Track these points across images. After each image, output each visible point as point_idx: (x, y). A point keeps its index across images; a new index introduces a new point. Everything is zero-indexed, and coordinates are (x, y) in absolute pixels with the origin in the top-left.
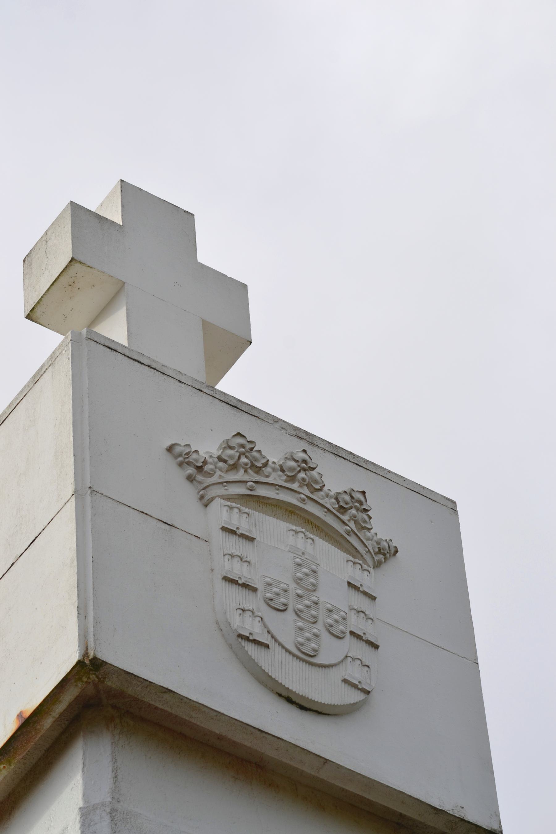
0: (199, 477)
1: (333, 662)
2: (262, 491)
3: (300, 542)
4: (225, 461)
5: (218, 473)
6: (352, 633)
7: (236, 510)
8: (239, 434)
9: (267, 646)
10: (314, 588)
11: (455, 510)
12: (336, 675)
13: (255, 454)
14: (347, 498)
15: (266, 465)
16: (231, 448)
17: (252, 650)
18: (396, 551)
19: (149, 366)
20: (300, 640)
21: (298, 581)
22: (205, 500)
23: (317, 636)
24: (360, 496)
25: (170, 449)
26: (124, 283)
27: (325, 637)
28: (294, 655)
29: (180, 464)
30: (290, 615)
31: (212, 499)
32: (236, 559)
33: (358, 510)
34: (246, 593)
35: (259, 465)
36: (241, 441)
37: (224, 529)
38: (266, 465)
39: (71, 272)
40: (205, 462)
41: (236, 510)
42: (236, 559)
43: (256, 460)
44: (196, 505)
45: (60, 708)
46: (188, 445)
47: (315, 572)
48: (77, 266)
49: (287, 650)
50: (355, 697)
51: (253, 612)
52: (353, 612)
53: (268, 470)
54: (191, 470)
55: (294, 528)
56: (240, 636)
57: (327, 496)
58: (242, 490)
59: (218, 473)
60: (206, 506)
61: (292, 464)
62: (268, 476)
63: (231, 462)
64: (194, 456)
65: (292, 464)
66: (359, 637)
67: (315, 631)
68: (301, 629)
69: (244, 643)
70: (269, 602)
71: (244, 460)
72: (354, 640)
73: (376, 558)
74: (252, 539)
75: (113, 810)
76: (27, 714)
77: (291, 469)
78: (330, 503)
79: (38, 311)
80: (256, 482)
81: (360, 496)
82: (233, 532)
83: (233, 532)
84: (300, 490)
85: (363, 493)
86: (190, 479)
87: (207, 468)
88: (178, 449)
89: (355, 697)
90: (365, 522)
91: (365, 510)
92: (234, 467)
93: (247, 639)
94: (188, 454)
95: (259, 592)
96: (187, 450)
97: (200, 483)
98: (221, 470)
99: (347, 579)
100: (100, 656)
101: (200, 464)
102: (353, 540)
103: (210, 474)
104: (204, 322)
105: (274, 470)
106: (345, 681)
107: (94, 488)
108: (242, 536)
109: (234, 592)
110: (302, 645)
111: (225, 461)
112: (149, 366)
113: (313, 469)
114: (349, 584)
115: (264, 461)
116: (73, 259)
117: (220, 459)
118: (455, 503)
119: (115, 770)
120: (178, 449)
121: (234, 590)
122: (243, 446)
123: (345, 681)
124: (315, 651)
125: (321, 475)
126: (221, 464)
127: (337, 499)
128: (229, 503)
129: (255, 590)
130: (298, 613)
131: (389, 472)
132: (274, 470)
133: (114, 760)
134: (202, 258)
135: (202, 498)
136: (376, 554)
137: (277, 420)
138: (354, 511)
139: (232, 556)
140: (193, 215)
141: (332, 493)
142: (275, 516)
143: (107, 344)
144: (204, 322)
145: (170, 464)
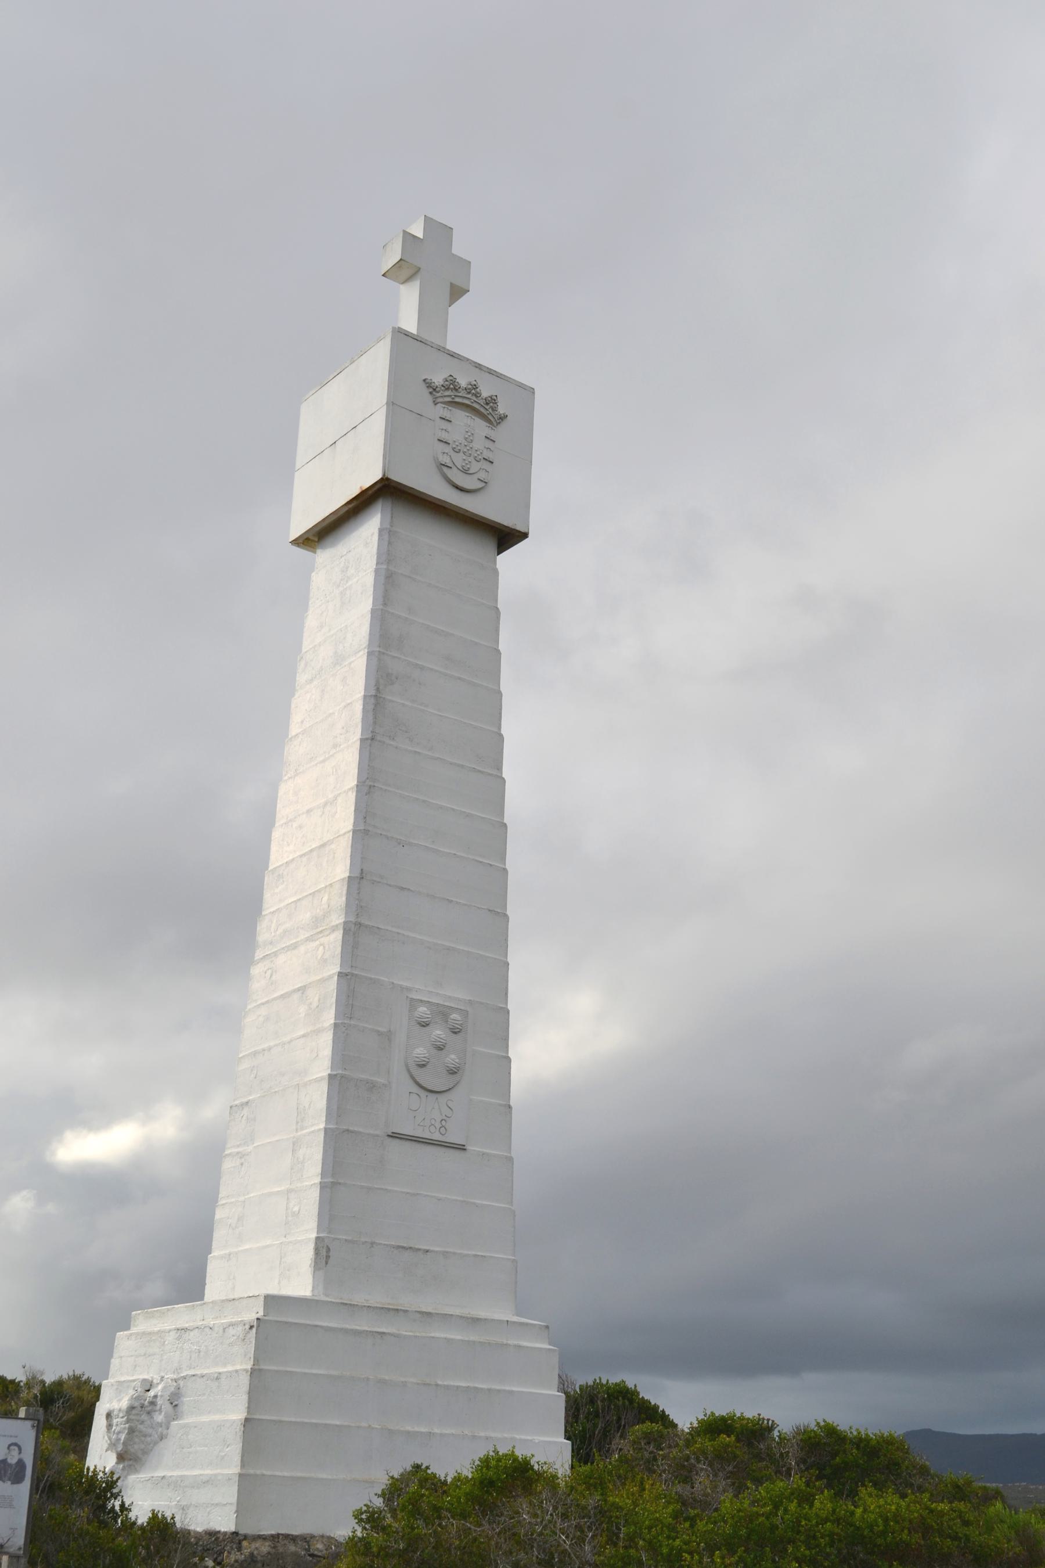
0: (434, 393)
1: (476, 471)
2: (457, 400)
3: (469, 421)
4: (444, 387)
5: (441, 392)
6: (484, 458)
7: (446, 409)
8: (451, 376)
9: (451, 468)
10: (472, 441)
11: (534, 393)
12: (476, 476)
13: (456, 384)
14: (490, 399)
15: (460, 388)
16: (447, 381)
17: (445, 469)
18: (507, 416)
19: (421, 341)
20: (464, 464)
21: (466, 439)
22: (436, 402)
23: (470, 462)
24: (495, 398)
25: (424, 380)
26: (420, 269)
27: (474, 462)
28: (461, 471)
29: (428, 387)
30: (461, 454)
31: (438, 403)
32: (443, 431)
33: (493, 403)
34: (446, 445)
35: (457, 388)
36: (451, 378)
37: (441, 418)
38: (460, 388)
39: (400, 263)
40: (437, 387)
41: (446, 409)
42: (443, 431)
43: (456, 386)
44: (432, 404)
45: (375, 488)
46: (431, 380)
47: (472, 434)
48: (402, 262)
49: (458, 468)
50: (481, 485)
51: (447, 453)
52: (485, 449)
53: (460, 390)
54: (431, 390)
55: (467, 414)
56: (441, 464)
57: (482, 399)
58: (449, 399)
59: (441, 392)
60: (436, 404)
61: (470, 387)
62: (460, 392)
63: (446, 387)
64: (433, 384)
65: (470, 387)
66: (486, 460)
67: (470, 460)
68: (464, 460)
69: (442, 467)
70: (453, 449)
71: (452, 386)
72: (484, 461)
73: (498, 421)
74: (450, 421)
75: (390, 531)
76: (364, 489)
77: (469, 389)
78: (482, 402)
79: (387, 274)
80: (455, 396)
81: (495, 398)
82: (444, 419)
83: (444, 419)
84: (471, 398)
85: (496, 396)
86: (431, 393)
87: (438, 389)
88: (427, 381)
89: (481, 485)
90: (495, 408)
91: (496, 403)
92: (448, 389)
93: (444, 465)
94: (431, 383)
95: (451, 445)
96: (430, 381)
97: (434, 395)
98: (442, 390)
99: (485, 435)
100: (389, 477)
101: (435, 388)
102: (490, 417)
103: (438, 392)
104: (451, 284)
105: (463, 390)
106: (479, 479)
107: (394, 402)
108: (447, 420)
109: (442, 445)
110: (464, 466)
111: (444, 387)
112: (421, 341)
113: (477, 388)
114: (486, 437)
115: (459, 386)
116: (401, 259)
117: (442, 386)
118: (534, 389)
119: (392, 514)
120: (427, 381)
121: (442, 444)
122: (452, 380)
123: (479, 479)
124: (469, 468)
125: (480, 390)
126: (443, 388)
127: (486, 400)
128: (444, 406)
129: (449, 444)
130: (464, 453)
131: (510, 378)
132: (463, 390)
133: (392, 510)
134: (456, 250)
135: (434, 401)
136: (498, 419)
137: (468, 360)
138: (491, 404)
139: (442, 429)
140: (452, 229)
141: (484, 398)
142: (461, 410)
143: (406, 333)
144: (451, 284)
145: (424, 386)
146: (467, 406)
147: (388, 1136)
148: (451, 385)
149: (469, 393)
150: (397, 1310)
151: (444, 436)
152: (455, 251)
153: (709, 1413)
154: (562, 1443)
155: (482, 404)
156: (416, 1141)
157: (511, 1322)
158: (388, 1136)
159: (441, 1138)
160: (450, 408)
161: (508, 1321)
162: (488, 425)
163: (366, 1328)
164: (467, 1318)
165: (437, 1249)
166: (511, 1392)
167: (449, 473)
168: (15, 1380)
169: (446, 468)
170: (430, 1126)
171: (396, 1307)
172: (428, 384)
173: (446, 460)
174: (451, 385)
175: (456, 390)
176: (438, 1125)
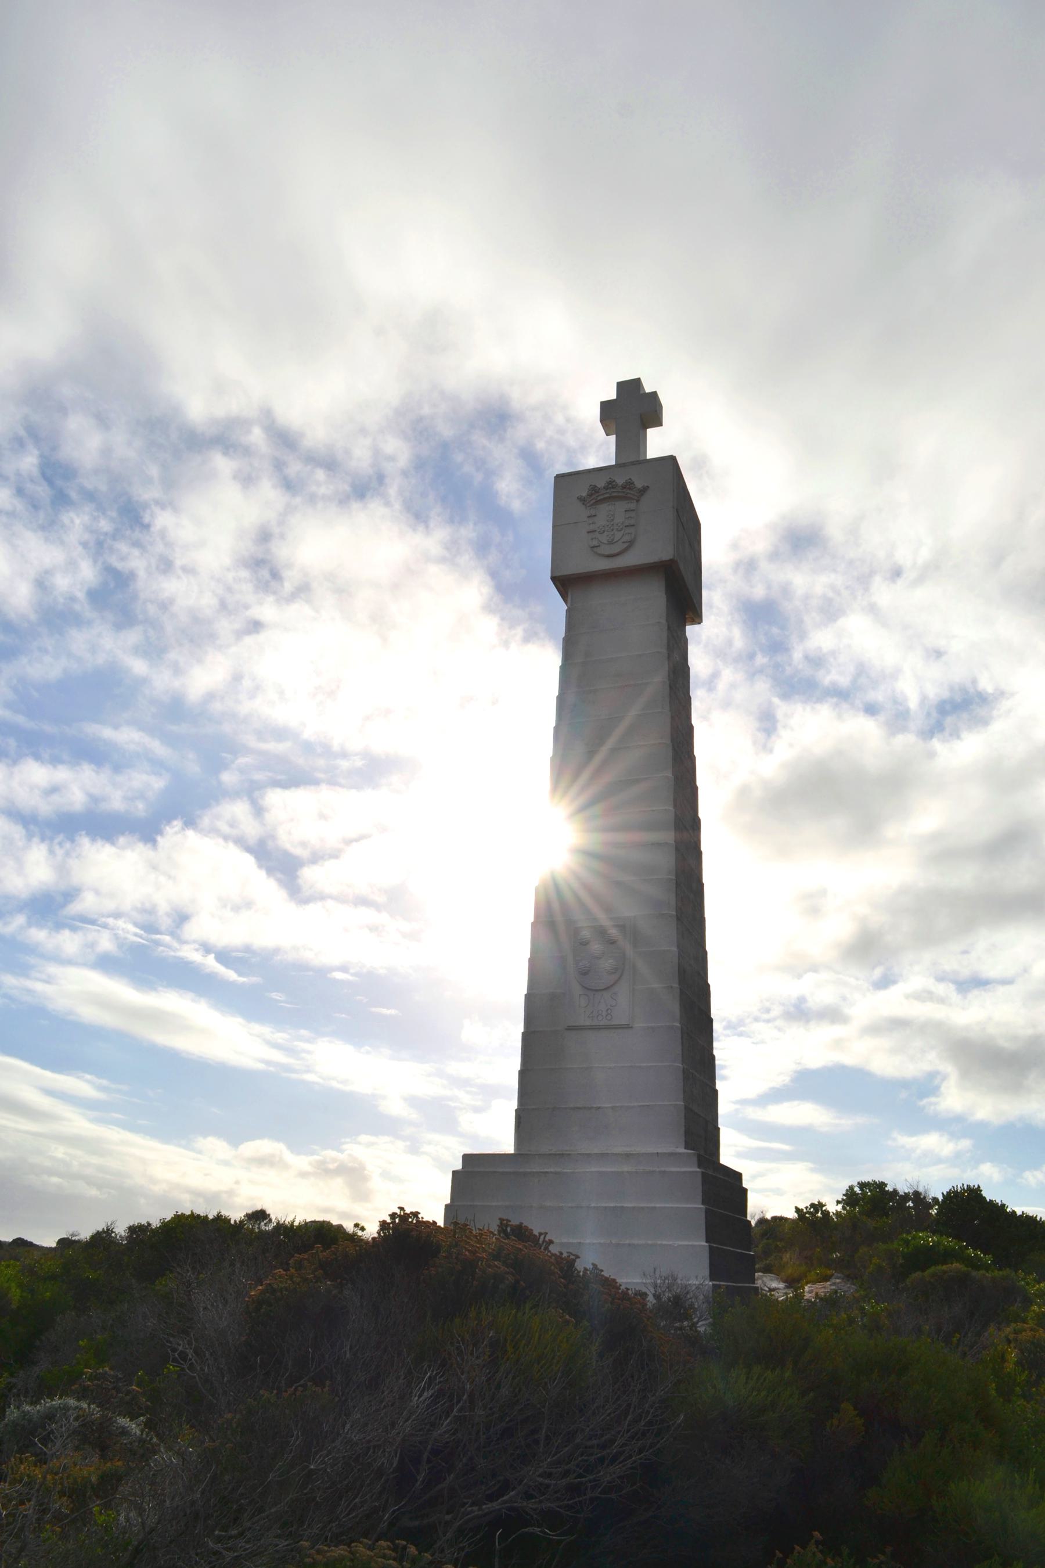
2: (599, 498)
17: (595, 549)
58: (594, 501)
102: (629, 495)
129: (595, 531)
146: (609, 498)
147: (566, 1029)
148: (594, 490)
149: (607, 489)
150: (563, 1154)
151: (592, 527)
152: (615, 397)
153: (230, 1217)
154: (704, 1245)
155: (620, 490)
156: (589, 1029)
157: (661, 1153)
158: (566, 1029)
159: (608, 1023)
160: (613, 503)
161: (658, 1153)
162: (627, 502)
163: (538, 1170)
164: (622, 1155)
165: (607, 1105)
166: (655, 1207)
167: (600, 550)
168: (1033, 1216)
169: (595, 548)
170: (598, 1016)
171: (568, 1153)
172: (582, 500)
173: (595, 543)
174: (594, 490)
175: (598, 492)
176: (604, 1014)
